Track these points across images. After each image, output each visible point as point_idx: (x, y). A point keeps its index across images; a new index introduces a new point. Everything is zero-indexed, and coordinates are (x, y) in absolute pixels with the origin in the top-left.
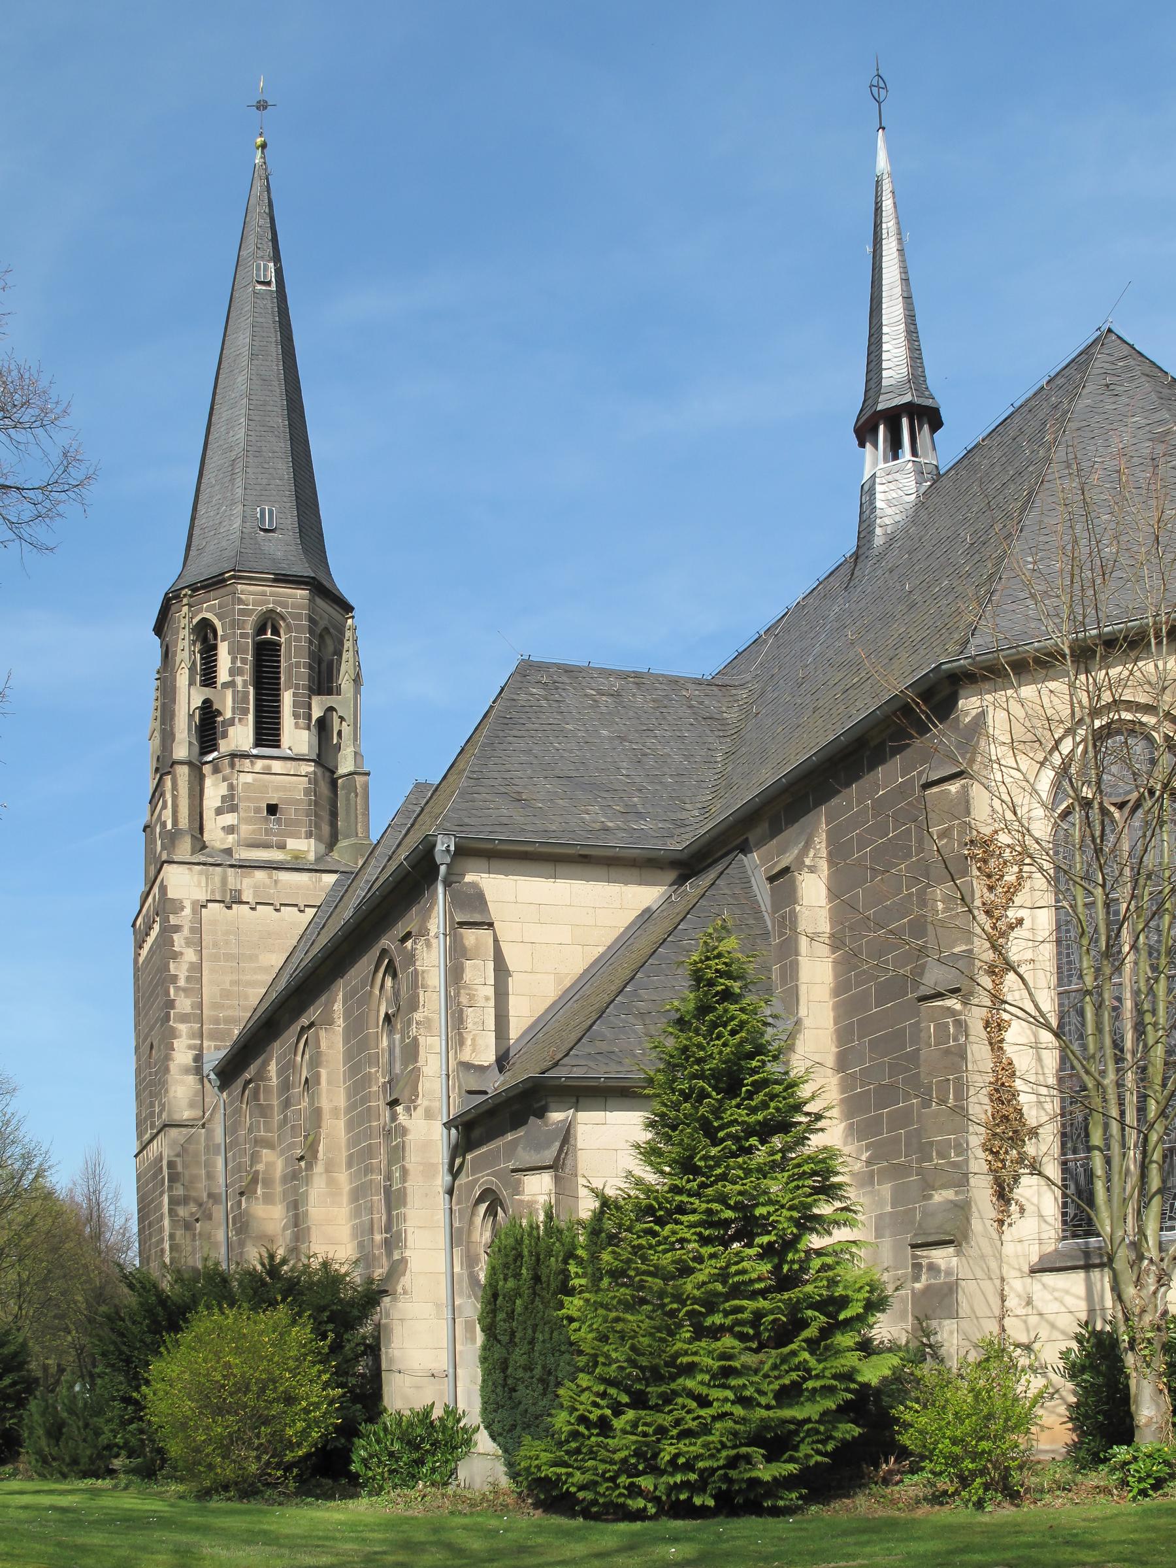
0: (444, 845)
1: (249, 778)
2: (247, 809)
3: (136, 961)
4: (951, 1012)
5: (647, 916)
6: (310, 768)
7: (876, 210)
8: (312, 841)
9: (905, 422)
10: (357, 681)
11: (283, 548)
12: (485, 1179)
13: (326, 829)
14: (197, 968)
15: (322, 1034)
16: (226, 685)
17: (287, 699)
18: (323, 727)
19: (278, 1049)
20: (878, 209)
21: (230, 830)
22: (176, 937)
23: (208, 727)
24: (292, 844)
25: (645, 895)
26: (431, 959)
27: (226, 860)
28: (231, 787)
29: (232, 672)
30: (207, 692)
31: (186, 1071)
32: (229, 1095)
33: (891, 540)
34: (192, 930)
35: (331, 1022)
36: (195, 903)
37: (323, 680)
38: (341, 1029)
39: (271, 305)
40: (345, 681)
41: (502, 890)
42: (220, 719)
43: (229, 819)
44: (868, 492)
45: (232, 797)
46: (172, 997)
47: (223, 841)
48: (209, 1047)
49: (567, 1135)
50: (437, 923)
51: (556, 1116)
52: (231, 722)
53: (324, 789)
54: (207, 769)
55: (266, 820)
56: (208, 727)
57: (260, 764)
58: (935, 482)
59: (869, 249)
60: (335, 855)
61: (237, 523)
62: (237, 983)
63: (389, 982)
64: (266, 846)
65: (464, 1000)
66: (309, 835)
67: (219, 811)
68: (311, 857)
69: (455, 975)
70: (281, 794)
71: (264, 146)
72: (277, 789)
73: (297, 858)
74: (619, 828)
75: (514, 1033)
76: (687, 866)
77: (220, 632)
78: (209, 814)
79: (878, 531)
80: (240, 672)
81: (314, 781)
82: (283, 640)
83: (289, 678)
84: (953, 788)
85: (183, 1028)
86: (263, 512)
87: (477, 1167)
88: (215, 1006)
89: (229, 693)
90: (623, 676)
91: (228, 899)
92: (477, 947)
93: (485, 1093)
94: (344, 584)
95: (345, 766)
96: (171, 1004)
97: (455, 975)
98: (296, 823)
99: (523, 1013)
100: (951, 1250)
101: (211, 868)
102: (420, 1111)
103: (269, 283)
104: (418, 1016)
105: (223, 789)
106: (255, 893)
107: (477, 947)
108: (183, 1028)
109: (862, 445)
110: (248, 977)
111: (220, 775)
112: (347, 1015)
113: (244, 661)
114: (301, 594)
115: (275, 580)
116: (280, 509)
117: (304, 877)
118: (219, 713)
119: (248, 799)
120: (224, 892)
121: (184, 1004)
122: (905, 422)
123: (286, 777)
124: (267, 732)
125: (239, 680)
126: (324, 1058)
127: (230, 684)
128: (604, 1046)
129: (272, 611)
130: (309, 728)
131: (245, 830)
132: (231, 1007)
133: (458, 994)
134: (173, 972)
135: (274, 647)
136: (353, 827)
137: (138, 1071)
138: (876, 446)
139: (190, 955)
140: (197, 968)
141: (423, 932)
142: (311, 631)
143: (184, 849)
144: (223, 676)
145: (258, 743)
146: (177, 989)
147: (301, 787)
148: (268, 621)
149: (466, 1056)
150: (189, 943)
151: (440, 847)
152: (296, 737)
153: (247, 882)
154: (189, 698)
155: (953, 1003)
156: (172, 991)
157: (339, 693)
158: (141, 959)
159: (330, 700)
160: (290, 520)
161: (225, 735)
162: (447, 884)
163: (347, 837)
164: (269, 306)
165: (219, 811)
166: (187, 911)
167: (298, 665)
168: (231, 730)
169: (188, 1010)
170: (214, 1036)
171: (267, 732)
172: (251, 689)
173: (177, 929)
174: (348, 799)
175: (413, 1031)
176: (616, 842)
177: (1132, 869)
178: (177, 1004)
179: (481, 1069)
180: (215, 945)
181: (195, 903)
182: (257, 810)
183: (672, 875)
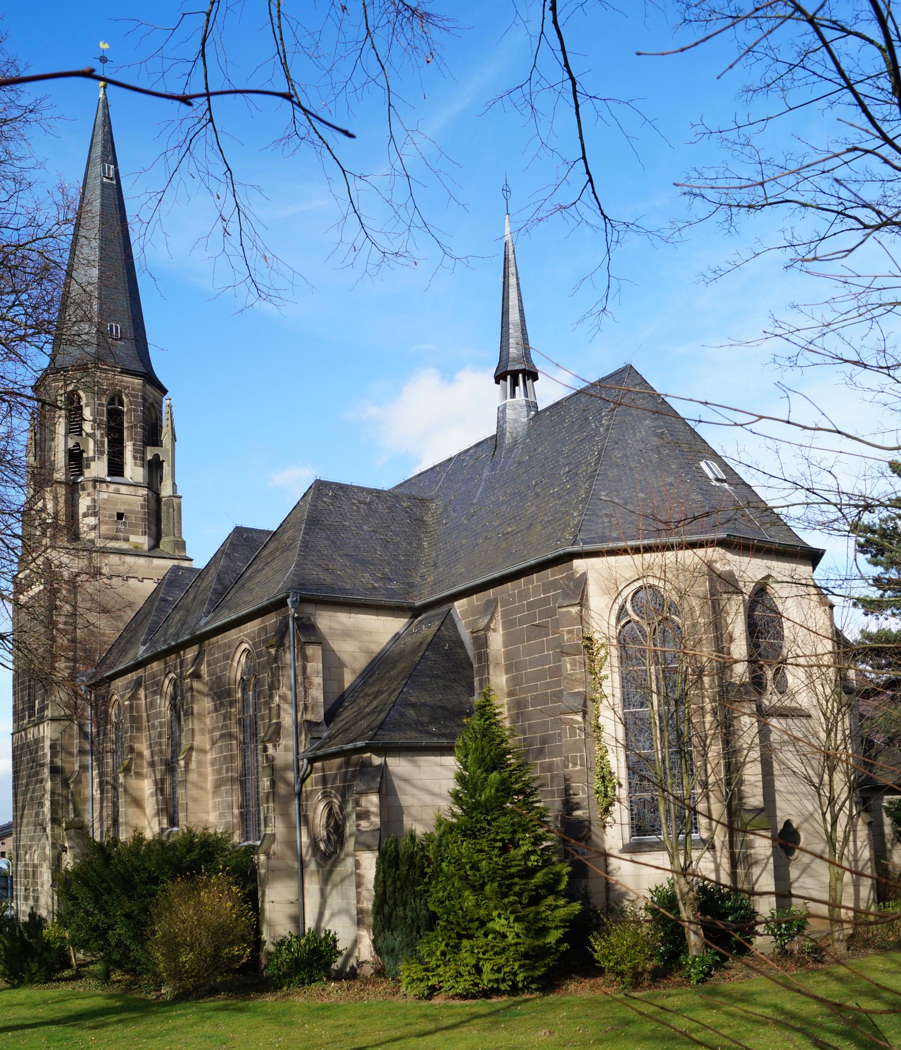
6: (144, 492)
7: (505, 259)
8: (146, 537)
9: (520, 375)
10: (174, 439)
13: (154, 528)
23: (76, 458)
24: (133, 538)
28: (94, 501)
30: (78, 439)
33: (515, 442)
40: (166, 438)
52: (93, 459)
56: (76, 458)
57: (112, 487)
59: (501, 280)
64: (116, 539)
66: (144, 533)
68: (146, 547)
70: (126, 507)
72: (123, 503)
73: (136, 548)
74: (381, 587)
76: (415, 612)
81: (147, 500)
86: (111, 327)
92: (313, 656)
93: (320, 738)
95: (166, 491)
98: (136, 525)
102: (282, 747)
107: (313, 656)
114: (137, 382)
117: (141, 561)
122: (520, 375)
123: (129, 495)
124: (116, 468)
125: (98, 434)
130: (143, 466)
131: (104, 529)
136: (172, 529)
142: (144, 406)
145: (110, 474)
147: (139, 503)
152: (133, 471)
154: (60, 444)
159: (156, 450)
161: (88, 467)
163: (168, 535)
164: (112, 193)
168: (93, 464)
171: (116, 468)
172: (106, 440)
174: (168, 512)
176: (380, 598)
177: (805, 940)
183: (410, 614)
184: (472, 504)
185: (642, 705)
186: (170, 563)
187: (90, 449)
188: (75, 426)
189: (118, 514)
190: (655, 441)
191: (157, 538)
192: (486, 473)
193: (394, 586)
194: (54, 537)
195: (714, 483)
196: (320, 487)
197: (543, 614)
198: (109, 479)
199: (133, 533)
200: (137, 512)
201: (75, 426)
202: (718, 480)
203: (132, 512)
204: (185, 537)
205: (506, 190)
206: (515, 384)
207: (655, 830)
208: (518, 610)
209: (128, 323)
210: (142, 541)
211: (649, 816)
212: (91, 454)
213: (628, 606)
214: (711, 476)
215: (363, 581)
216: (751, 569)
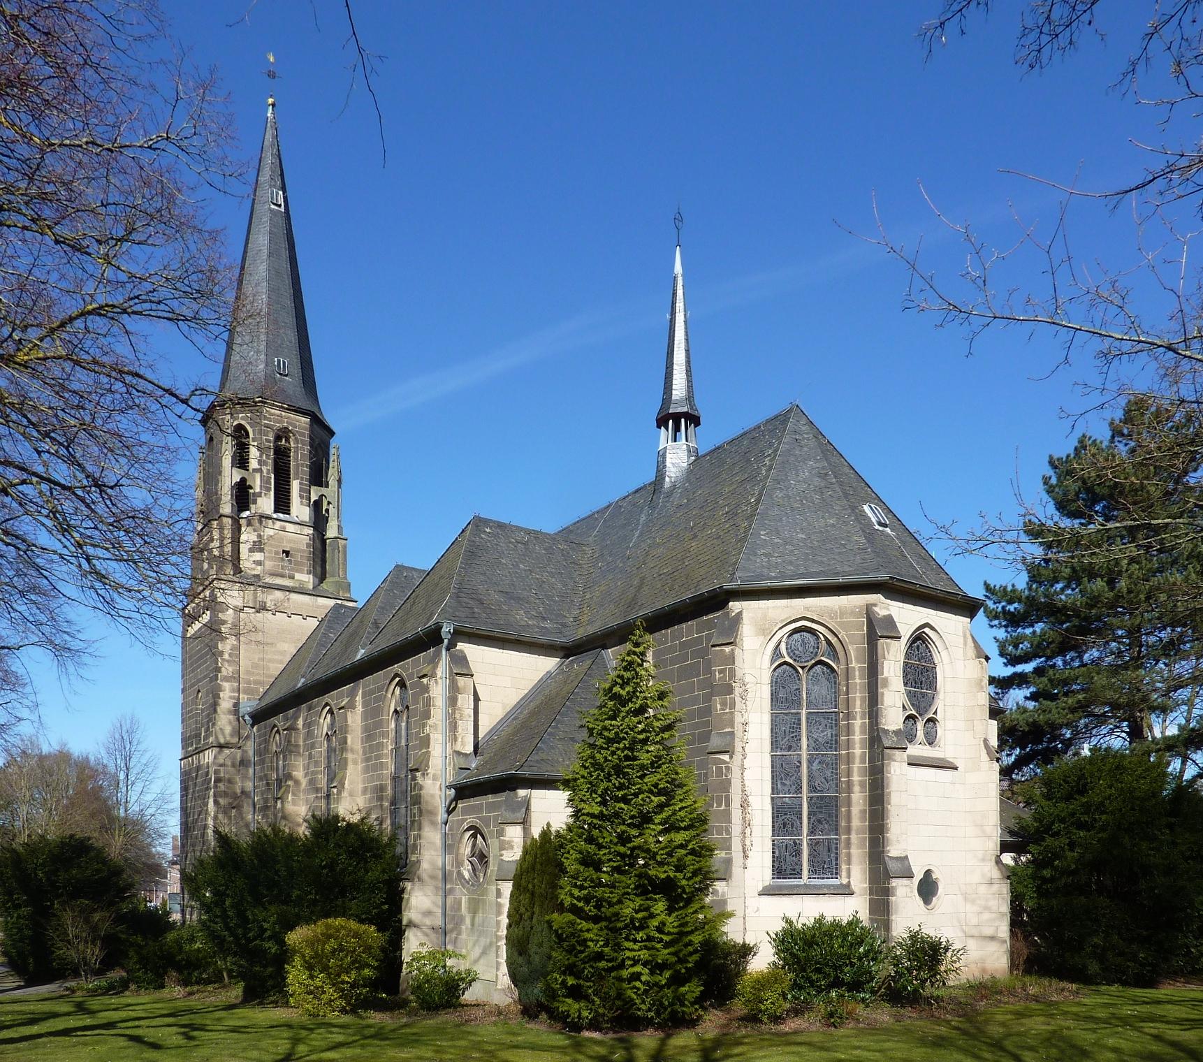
0: (446, 629)
1: (271, 532)
2: (270, 552)
4: (724, 762)
5: (549, 675)
11: (292, 383)
12: (471, 820)
13: (319, 569)
15: (349, 714)
16: (255, 470)
17: (295, 486)
18: (317, 506)
20: (675, 294)
21: (259, 563)
23: (243, 495)
24: (298, 576)
25: (548, 664)
26: (438, 690)
27: (254, 582)
28: (259, 536)
30: (243, 473)
31: (230, 712)
32: (258, 730)
33: (674, 486)
37: (317, 476)
39: (281, 222)
40: (332, 479)
41: (472, 652)
43: (258, 556)
44: (662, 455)
49: (527, 804)
50: (442, 669)
51: (522, 793)
52: (260, 495)
53: (319, 545)
54: (243, 522)
55: (283, 560)
56: (243, 495)
57: (278, 524)
58: (698, 460)
59: (668, 317)
60: (324, 585)
61: (262, 366)
62: (263, 659)
63: (398, 691)
64: (282, 576)
65: (457, 716)
69: (452, 701)
71: (273, 105)
72: (289, 541)
75: (481, 736)
76: (568, 651)
77: (251, 435)
78: (244, 549)
79: (667, 479)
80: (266, 464)
83: (297, 473)
84: (727, 649)
85: (226, 685)
87: (466, 811)
88: (248, 672)
89: (258, 476)
90: (528, 532)
94: (330, 419)
95: (331, 532)
96: (218, 670)
97: (452, 701)
98: (301, 564)
99: (485, 726)
100: (724, 883)
104: (430, 722)
108: (226, 685)
109: (659, 427)
112: (365, 704)
114: (305, 420)
116: (288, 361)
118: (251, 487)
121: (227, 670)
124: (282, 504)
125: (264, 469)
127: (260, 471)
128: (544, 756)
131: (269, 565)
133: (454, 713)
137: (184, 706)
138: (667, 429)
141: (434, 675)
143: (229, 570)
144: (253, 464)
148: (282, 434)
149: (458, 747)
151: (445, 629)
152: (300, 510)
153: (270, 597)
154: (230, 476)
155: (726, 757)
157: (327, 486)
159: (323, 490)
160: (297, 371)
161: (255, 502)
162: (448, 649)
165: (251, 550)
167: (302, 465)
168: (259, 500)
170: (247, 691)
171: (282, 504)
173: (224, 622)
175: (427, 730)
176: (537, 636)
179: (466, 755)
184: (628, 548)
185: (790, 748)
186: (332, 602)
187: (256, 484)
188: (241, 461)
189: (284, 552)
190: (817, 481)
191: (322, 577)
192: (643, 518)
193: (548, 624)
194: (220, 569)
195: (877, 527)
196: (478, 523)
197: (695, 654)
198: (275, 516)
199: (298, 571)
200: (303, 551)
201: (241, 461)
202: (880, 524)
203: (299, 551)
204: (350, 578)
205: (679, 218)
206: (677, 429)
207: (797, 874)
208: (671, 650)
209: (296, 360)
210: (307, 579)
211: (790, 859)
212: (258, 490)
213: (783, 647)
214: (874, 520)
215: (521, 620)
216: (908, 616)
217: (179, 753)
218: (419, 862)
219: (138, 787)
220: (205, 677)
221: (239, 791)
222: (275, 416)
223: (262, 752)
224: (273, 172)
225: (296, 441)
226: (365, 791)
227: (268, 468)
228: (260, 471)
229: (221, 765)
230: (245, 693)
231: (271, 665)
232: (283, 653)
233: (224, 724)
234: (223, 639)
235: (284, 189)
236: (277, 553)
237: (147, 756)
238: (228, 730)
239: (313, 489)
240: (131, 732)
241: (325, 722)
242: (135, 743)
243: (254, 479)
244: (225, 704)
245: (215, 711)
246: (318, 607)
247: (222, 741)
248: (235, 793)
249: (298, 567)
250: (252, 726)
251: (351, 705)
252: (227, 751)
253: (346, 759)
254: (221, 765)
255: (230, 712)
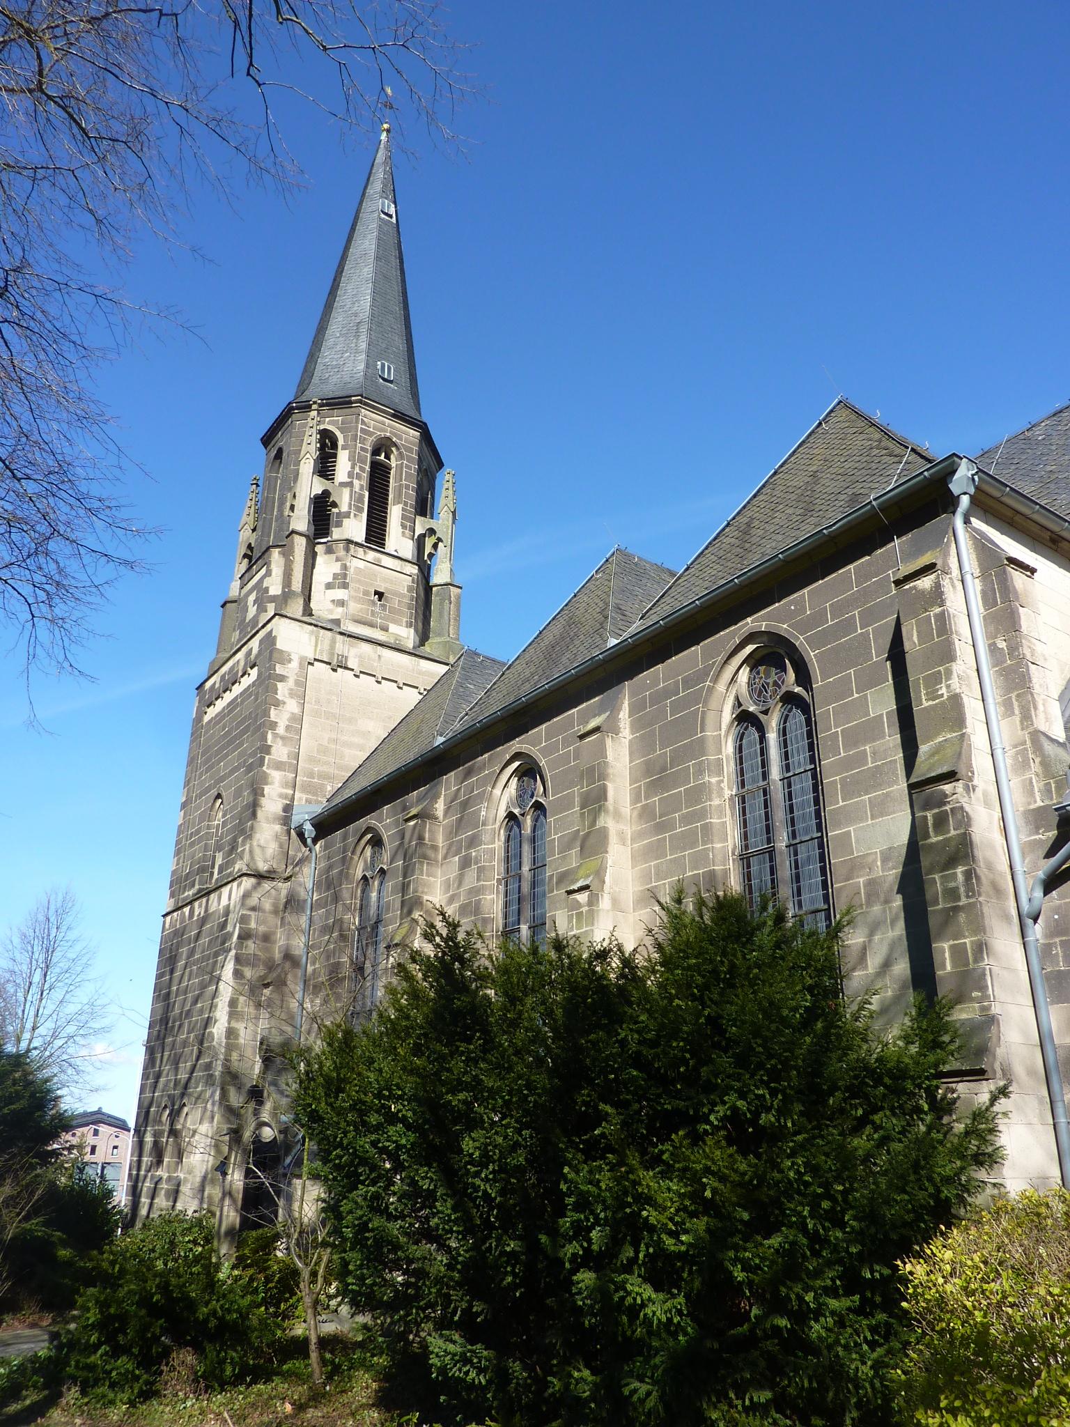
3: (199, 719)
8: (412, 630)
11: (397, 393)
13: (420, 625)
14: (298, 719)
15: (609, 742)
16: (342, 484)
17: (395, 514)
19: (450, 782)
21: (341, 603)
22: (280, 685)
23: (322, 510)
24: (393, 628)
28: (345, 567)
29: (350, 475)
32: (326, 847)
34: (297, 683)
35: (616, 731)
36: (302, 659)
38: (627, 742)
42: (335, 510)
43: (340, 594)
45: (345, 576)
46: (269, 743)
47: (331, 612)
48: (300, 799)
52: (347, 515)
54: (319, 549)
55: (374, 603)
56: (322, 510)
62: (336, 741)
64: (372, 625)
66: (409, 625)
67: (329, 586)
70: (388, 585)
71: (388, 131)
72: (384, 580)
77: (341, 442)
82: (393, 465)
86: (383, 366)
88: (311, 759)
89: (346, 491)
91: (335, 662)
96: (267, 749)
98: (399, 612)
101: (322, 631)
103: (391, 216)
105: (336, 568)
106: (360, 664)
110: (345, 738)
111: (333, 556)
112: (634, 727)
113: (362, 469)
114: (414, 434)
115: (394, 416)
118: (334, 505)
119: (359, 581)
120: (332, 654)
121: (280, 752)
124: (376, 534)
125: (356, 482)
126: (610, 771)
129: (389, 439)
131: (354, 607)
132: (327, 763)
134: (273, 718)
135: (387, 469)
139: (292, 706)
140: (298, 719)
143: (296, 608)
146: (276, 736)
147: (405, 584)
148: (383, 446)
150: (292, 694)
152: (398, 540)
154: (308, 485)
156: (270, 736)
158: (206, 718)
159: (432, 524)
160: (405, 380)
161: (339, 525)
163: (440, 635)
165: (329, 586)
166: (294, 665)
167: (407, 487)
168: (346, 522)
169: (284, 758)
170: (307, 788)
172: (367, 494)
173: (282, 678)
178: (273, 750)
180: (318, 702)
181: (302, 659)
182: (366, 593)
187: (344, 500)
188: (325, 468)
189: (376, 593)
200: (401, 595)
201: (325, 468)
203: (396, 594)
210: (408, 636)
217: (167, 904)
218: (990, 1021)
219: (57, 994)
220: (236, 769)
221: (278, 956)
222: (375, 423)
223: (330, 884)
224: (385, 185)
225: (401, 456)
226: (640, 902)
227: (361, 484)
228: (350, 484)
229: (253, 909)
230: (304, 790)
231: (347, 751)
232: (366, 734)
233: (266, 841)
234: (277, 704)
235: (395, 203)
236: (366, 593)
237: (78, 947)
238: (272, 848)
239: (419, 519)
240: (62, 912)
241: (503, 795)
242: (64, 928)
243: (341, 496)
244: (271, 804)
245: (254, 815)
246: (420, 673)
247: (263, 867)
248: (271, 960)
249: (394, 615)
250: (315, 841)
251: (611, 728)
252: (267, 885)
253: (603, 834)
254: (253, 909)
255: (276, 819)
